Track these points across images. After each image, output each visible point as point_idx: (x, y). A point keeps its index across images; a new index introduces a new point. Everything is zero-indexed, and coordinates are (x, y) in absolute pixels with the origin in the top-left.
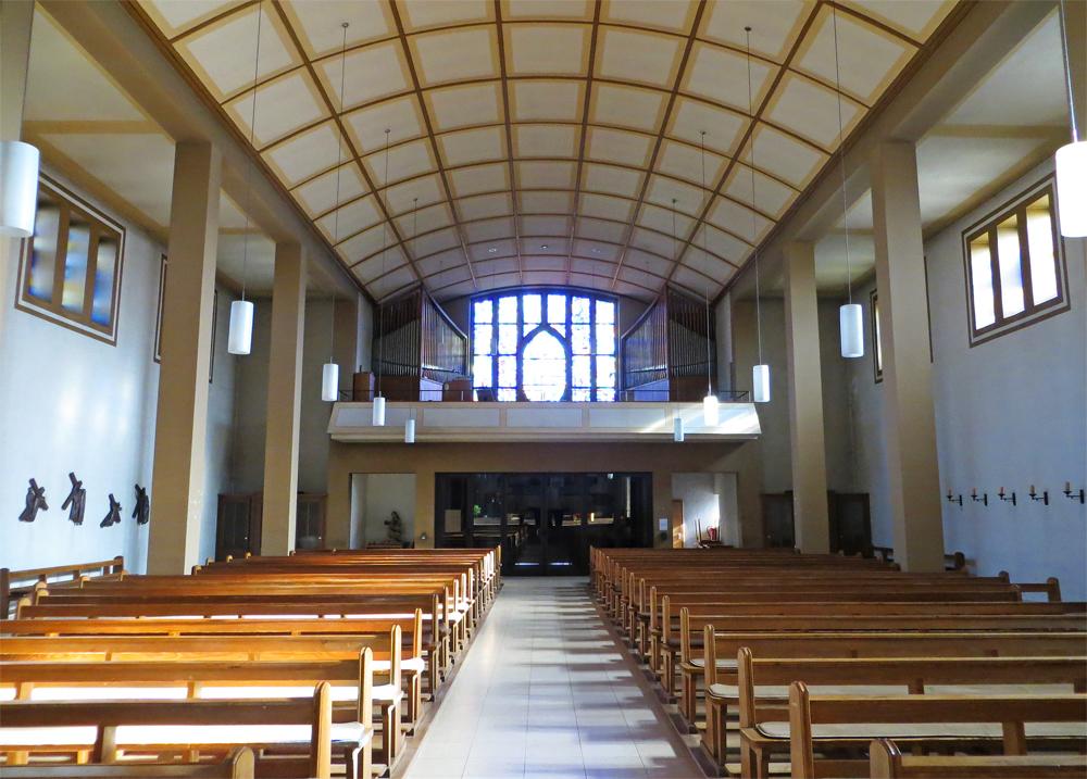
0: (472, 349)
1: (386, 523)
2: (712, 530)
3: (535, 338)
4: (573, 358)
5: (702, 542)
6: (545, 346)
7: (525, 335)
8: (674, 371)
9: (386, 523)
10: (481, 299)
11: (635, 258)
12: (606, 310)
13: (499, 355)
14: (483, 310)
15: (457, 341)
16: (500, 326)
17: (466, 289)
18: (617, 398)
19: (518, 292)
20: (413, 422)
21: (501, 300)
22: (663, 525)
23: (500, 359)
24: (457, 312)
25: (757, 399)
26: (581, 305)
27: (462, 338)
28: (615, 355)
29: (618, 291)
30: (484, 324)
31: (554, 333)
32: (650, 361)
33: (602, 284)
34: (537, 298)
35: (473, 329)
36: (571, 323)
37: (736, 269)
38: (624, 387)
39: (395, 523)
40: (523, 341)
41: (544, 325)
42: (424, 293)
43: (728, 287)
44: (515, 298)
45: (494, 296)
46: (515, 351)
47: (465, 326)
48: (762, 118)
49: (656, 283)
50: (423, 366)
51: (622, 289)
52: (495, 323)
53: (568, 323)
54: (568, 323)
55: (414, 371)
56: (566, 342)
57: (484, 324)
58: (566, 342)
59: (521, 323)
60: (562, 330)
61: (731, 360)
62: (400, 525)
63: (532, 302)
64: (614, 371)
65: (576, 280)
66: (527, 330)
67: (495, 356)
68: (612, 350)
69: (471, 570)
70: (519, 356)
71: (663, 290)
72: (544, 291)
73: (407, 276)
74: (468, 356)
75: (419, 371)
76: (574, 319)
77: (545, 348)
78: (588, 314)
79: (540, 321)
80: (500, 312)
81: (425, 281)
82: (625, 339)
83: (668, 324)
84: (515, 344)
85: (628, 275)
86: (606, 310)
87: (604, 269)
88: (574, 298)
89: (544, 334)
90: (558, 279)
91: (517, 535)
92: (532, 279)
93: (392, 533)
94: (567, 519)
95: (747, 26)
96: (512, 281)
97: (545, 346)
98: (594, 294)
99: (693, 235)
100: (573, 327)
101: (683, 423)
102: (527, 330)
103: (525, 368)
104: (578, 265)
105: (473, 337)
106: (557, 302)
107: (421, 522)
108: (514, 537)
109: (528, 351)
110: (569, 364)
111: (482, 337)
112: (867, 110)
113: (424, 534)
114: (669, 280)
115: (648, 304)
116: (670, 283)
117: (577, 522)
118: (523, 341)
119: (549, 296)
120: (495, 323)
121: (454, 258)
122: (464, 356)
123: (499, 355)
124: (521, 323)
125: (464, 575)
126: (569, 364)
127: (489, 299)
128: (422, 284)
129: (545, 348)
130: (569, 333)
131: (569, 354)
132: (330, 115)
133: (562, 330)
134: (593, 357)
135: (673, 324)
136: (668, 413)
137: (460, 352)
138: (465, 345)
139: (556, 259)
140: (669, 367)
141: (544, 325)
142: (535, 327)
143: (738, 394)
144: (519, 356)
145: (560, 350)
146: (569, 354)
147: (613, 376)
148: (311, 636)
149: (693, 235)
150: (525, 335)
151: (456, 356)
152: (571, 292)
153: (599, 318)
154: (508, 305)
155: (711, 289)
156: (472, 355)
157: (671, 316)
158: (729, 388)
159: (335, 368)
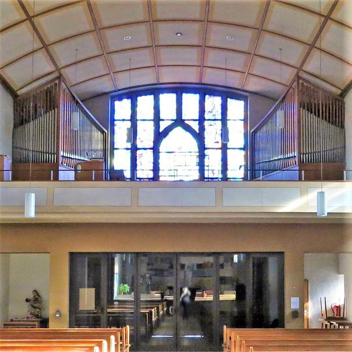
0: (113, 143)
1: (27, 300)
2: (337, 307)
3: (171, 134)
4: (206, 152)
5: (329, 319)
6: (179, 140)
7: (161, 130)
8: (303, 157)
9: (27, 300)
10: (120, 98)
11: (269, 45)
12: (236, 108)
13: (137, 149)
14: (122, 108)
15: (97, 135)
16: (139, 123)
17: (105, 85)
19: (155, 91)
20: (33, 195)
21: (139, 98)
22: (293, 303)
23: (139, 152)
24: (98, 107)
25: (225, 263)
26: (213, 103)
27: (103, 132)
28: (244, 149)
30: (123, 120)
31: (188, 128)
33: (234, 80)
34: (173, 97)
35: (113, 125)
36: (205, 120)
39: (36, 300)
40: (159, 136)
41: (179, 121)
42: (63, 84)
44: (152, 97)
45: (133, 94)
46: (151, 145)
47: (107, 123)
48: (331, 17)
49: (287, 75)
50: (61, 153)
51: (253, 85)
52: (133, 119)
53: (201, 120)
54: (201, 120)
55: (53, 158)
56: (200, 137)
57: (123, 120)
58: (200, 137)
59: (157, 119)
60: (195, 126)
62: (40, 302)
63: (168, 101)
64: (243, 163)
65: (211, 77)
66: (163, 126)
67: (134, 149)
68: (241, 144)
69: (113, 338)
70: (155, 150)
71: (293, 81)
72: (179, 90)
73: (42, 65)
74: (109, 148)
75: (58, 158)
76: (207, 116)
77: (180, 142)
78: (220, 111)
79: (175, 118)
80: (138, 109)
81: (62, 71)
82: (255, 132)
83: (299, 111)
84: (152, 139)
85: (260, 66)
86: (236, 108)
87: (238, 62)
88: (207, 97)
89: (179, 130)
90: (191, 76)
91: (153, 310)
92: (168, 76)
93: (33, 310)
94: (199, 296)
96: (146, 78)
97: (179, 140)
98: (223, 92)
99: (318, 36)
100: (206, 123)
101: (327, 197)
102: (163, 126)
103: (161, 161)
104: (213, 58)
105: (113, 132)
106: (191, 101)
107: (57, 304)
108: (151, 313)
109: (165, 145)
110: (202, 156)
111: (121, 131)
113: (58, 311)
114: (300, 69)
115: (276, 100)
117: (211, 298)
118: (159, 136)
119: (184, 95)
120: (133, 119)
121: (98, 66)
122: (105, 151)
123: (137, 149)
124: (157, 119)
125: (105, 342)
126: (202, 156)
127: (128, 98)
128: (61, 75)
129: (180, 142)
130: (202, 128)
131: (202, 148)
132: (49, 47)
133: (195, 126)
134: (224, 148)
135: (304, 112)
136: (303, 192)
137: (100, 146)
138: (105, 141)
139: (188, 50)
140: (300, 153)
141: (179, 121)
142: (171, 122)
144: (155, 150)
145: (193, 144)
146: (202, 148)
147: (243, 168)
149: (318, 36)
150: (161, 130)
151: (95, 151)
152: (204, 90)
154: (145, 103)
156: (113, 149)
157: (302, 105)
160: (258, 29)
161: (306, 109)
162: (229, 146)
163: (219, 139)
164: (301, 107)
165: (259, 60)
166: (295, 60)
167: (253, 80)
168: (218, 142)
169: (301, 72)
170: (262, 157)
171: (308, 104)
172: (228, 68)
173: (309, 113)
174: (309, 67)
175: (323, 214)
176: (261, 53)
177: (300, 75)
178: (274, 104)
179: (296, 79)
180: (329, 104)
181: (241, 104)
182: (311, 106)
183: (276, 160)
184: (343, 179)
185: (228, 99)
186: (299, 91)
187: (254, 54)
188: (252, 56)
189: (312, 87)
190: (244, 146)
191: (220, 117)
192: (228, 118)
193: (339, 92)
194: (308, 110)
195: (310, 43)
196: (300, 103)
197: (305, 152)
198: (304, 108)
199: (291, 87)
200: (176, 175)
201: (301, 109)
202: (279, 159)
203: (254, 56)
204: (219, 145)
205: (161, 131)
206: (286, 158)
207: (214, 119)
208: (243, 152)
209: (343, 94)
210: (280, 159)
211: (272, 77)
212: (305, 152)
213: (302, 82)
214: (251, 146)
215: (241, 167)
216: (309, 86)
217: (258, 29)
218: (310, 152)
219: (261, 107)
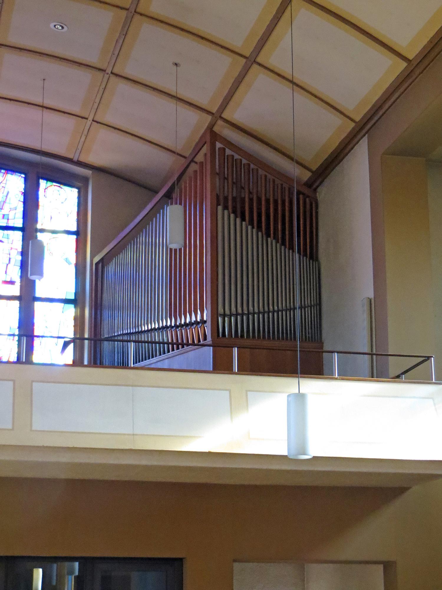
12: (59, 205)
18: (77, 362)
29: (92, 159)
32: (162, 298)
33: (55, 137)
37: (353, 125)
38: (97, 340)
43: (365, 126)
49: (182, 128)
51: (105, 150)
61: (368, 291)
85: (125, 105)
86: (59, 205)
95: (177, 62)
112: (404, 65)
114: (217, 116)
115: (156, 192)
116: (221, 129)
136: (236, 406)
140: (215, 315)
143: (395, 365)
148: (309, 337)
153: (43, 220)
155: (319, 132)
157: (220, 200)
158: (363, 344)
159: (41, 570)
160: (127, 9)
161: (230, 210)
162: (39, 293)
163: (15, 273)
164: (218, 204)
165: (123, 87)
166: (207, 94)
167: (103, 135)
168: (12, 283)
169: (220, 122)
170: (116, 324)
171: (234, 199)
172: (48, 102)
173: (238, 220)
174: (238, 113)
175: (305, 454)
176: (129, 72)
177: (216, 129)
178: (150, 200)
179: (208, 138)
180: (276, 202)
181: (71, 194)
182: (291, 193)
183: (155, 329)
184: (332, 373)
185: (43, 183)
186: (214, 173)
187: (112, 73)
188: (107, 76)
189: (244, 161)
190: (76, 294)
191: (19, 223)
192: (39, 226)
193: (306, 176)
194: (234, 212)
195: (247, 54)
196: (218, 197)
197: (256, 310)
198: (226, 207)
199: (192, 161)
200: (374, 357)
201: (220, 208)
202: (163, 328)
203: (113, 78)
204: (15, 290)
205: (365, 139)
206: (181, 326)
207: (5, 225)
208: (71, 310)
209: (315, 181)
210: (167, 327)
211: (148, 129)
212: (256, 310)
213: (221, 146)
214: (94, 297)
215: (66, 345)
216: (237, 157)
217: (127, 9)
218: (240, 311)
219: (120, 202)
